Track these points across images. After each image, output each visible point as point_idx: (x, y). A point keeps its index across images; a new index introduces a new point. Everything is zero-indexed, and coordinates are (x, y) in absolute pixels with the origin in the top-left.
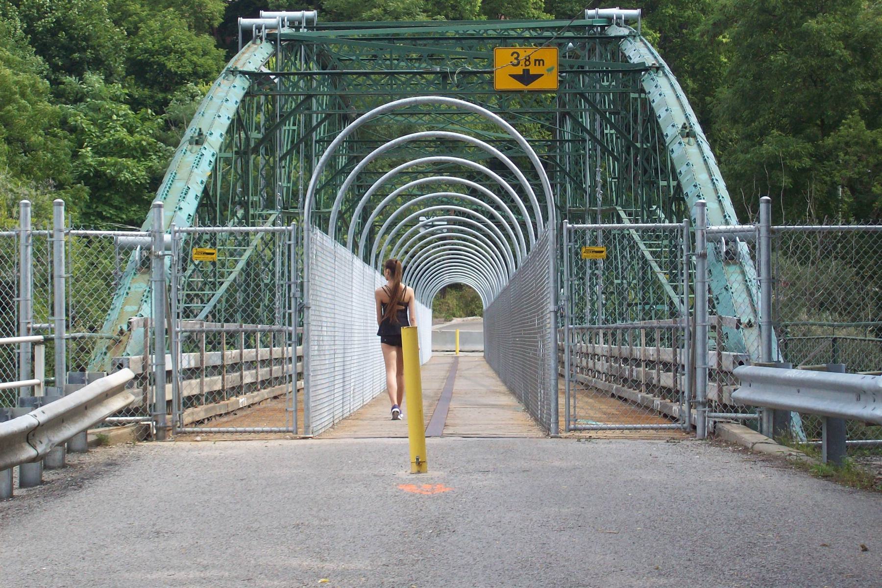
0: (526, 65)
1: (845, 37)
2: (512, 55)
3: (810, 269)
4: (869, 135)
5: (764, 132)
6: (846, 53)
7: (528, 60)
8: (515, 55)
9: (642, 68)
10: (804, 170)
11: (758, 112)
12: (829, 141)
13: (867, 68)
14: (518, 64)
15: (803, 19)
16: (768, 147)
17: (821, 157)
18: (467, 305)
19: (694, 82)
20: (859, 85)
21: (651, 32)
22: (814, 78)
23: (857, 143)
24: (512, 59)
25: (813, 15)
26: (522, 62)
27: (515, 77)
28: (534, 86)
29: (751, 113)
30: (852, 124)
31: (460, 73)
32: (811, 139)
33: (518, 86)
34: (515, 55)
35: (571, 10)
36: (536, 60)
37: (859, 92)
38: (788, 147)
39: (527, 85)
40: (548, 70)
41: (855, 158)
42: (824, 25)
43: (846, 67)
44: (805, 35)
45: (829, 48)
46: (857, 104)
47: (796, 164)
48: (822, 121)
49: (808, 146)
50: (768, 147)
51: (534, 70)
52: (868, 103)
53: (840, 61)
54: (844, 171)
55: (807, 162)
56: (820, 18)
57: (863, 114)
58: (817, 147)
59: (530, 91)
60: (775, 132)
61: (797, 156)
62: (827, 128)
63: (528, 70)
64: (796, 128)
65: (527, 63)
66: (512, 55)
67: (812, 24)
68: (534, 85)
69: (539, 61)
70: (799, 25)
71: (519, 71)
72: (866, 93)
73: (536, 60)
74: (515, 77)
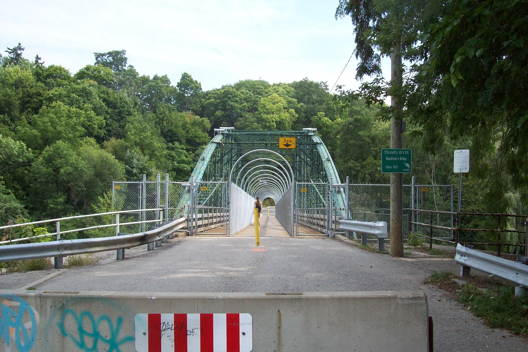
1: (369, 136)
10: (359, 170)
17: (363, 167)
18: (271, 203)
20: (372, 149)
22: (360, 147)
32: (360, 162)
44: (358, 136)
50: (350, 164)
55: (359, 168)
61: (357, 167)
62: (364, 159)
64: (356, 160)
67: (361, 133)
72: (374, 150)
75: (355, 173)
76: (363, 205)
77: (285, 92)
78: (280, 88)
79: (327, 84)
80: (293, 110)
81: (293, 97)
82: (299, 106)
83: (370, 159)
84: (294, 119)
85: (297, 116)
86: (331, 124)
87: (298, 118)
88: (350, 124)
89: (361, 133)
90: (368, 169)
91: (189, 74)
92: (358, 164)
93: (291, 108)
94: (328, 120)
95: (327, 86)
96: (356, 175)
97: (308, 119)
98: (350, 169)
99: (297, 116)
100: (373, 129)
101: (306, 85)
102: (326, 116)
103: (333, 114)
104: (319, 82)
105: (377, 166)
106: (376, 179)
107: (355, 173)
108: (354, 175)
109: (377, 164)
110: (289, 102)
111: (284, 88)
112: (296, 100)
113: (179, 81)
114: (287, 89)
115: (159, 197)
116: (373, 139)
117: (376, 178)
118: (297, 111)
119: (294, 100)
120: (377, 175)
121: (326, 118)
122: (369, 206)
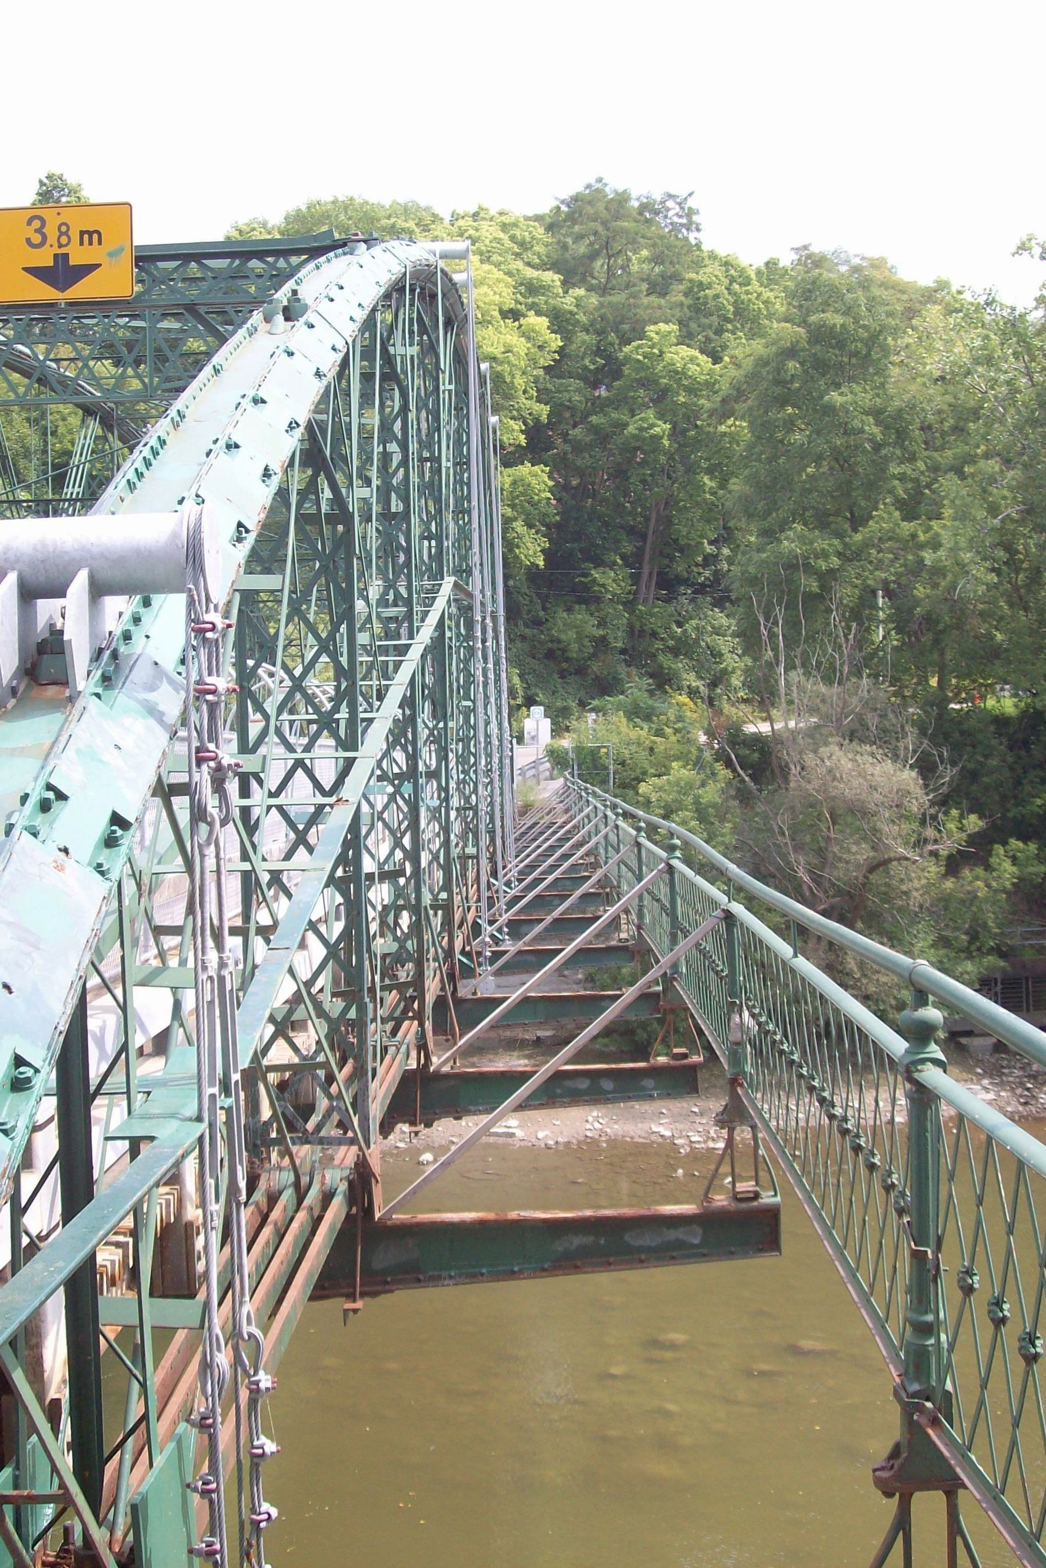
0: (60, 246)
1: (876, 413)
2: (30, 222)
3: (836, 689)
4: (907, 527)
5: (784, 525)
6: (876, 430)
7: (66, 233)
8: (37, 224)
10: (831, 572)
11: (776, 504)
12: (858, 537)
13: (904, 448)
14: (43, 243)
15: (826, 392)
16: (790, 544)
17: (851, 556)
19: (711, 480)
20: (895, 469)
21: (660, 423)
22: (841, 459)
23: (890, 539)
25: (837, 386)
26: (52, 239)
27: (36, 272)
28: (81, 290)
29: (1016, 687)
30: (885, 516)
32: (840, 535)
34: (37, 224)
35: (570, 401)
37: (894, 476)
38: (812, 543)
39: (63, 290)
40: (111, 255)
41: (891, 556)
42: (850, 397)
43: (877, 447)
44: (830, 410)
45: (856, 423)
46: (891, 492)
47: (823, 565)
48: (852, 514)
49: (836, 542)
50: (790, 544)
51: (78, 256)
52: (905, 491)
53: (870, 441)
54: (877, 573)
55: (835, 562)
56: (843, 389)
57: (900, 504)
58: (846, 545)
59: (73, 304)
60: (798, 527)
61: (824, 555)
62: (857, 522)
64: (822, 522)
65: (64, 240)
66: (30, 222)
67: (835, 397)
68: (83, 290)
69: (90, 234)
70: (821, 397)
71: (45, 258)
72: (902, 478)
74: (36, 272)
75: (815, 587)
76: (855, 734)
77: (508, 244)
78: (485, 225)
79: (691, 203)
80: (541, 323)
81: (543, 266)
82: (568, 302)
83: (886, 518)
84: (546, 360)
85: (556, 342)
86: (711, 373)
87: (561, 351)
88: (791, 352)
89: (835, 397)
90: (879, 565)
91: (71, 179)
92: (822, 543)
93: (539, 313)
94: (692, 359)
95: (691, 213)
96: (820, 597)
97: (609, 358)
98: (792, 565)
99: (556, 342)
100: (895, 371)
101: (601, 206)
102: (686, 338)
103: (719, 332)
104: (657, 196)
105: (922, 547)
106: (847, 540)
107: (815, 587)
108: (810, 598)
109: (922, 537)
110: (532, 288)
111: (504, 227)
112: (557, 277)
114: (517, 233)
115: (502, 620)
116: (896, 425)
117: (917, 602)
118: (560, 321)
119: (552, 278)
120: (920, 591)
121: (685, 351)
122: (885, 740)
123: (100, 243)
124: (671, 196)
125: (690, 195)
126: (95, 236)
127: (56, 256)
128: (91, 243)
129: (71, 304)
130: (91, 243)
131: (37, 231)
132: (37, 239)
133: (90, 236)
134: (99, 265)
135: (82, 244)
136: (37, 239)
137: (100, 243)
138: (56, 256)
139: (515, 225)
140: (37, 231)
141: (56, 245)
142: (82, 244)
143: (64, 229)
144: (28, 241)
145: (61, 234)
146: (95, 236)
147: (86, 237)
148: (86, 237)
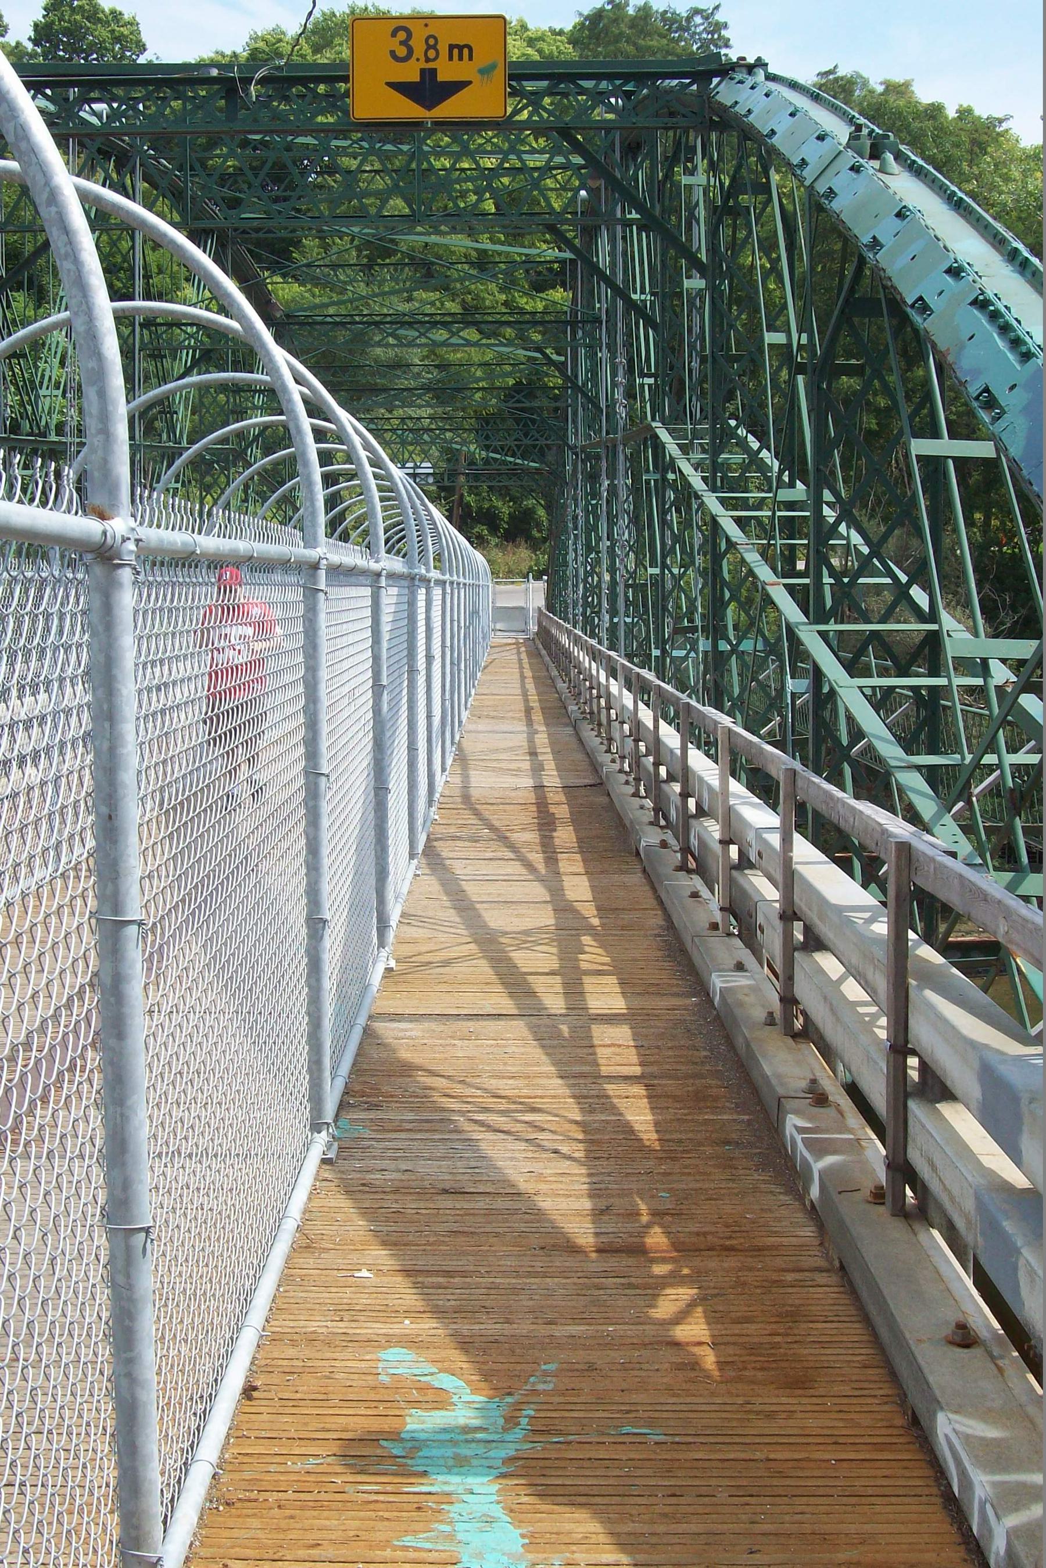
0: (428, 60)
2: (394, 34)
7: (434, 47)
8: (402, 35)
9: (713, 67)
24: (395, 44)
31: (262, 81)
33: (408, 109)
34: (402, 35)
36: (452, 47)
39: (429, 108)
51: (447, 71)
63: (433, 72)
65: (431, 54)
66: (394, 34)
69: (461, 48)
71: (411, 73)
73: (452, 47)
79: (719, 17)
113: (39, 15)
123: (471, 58)
124: (697, 11)
125: (717, 8)
126: (466, 51)
127: (423, 71)
128: (461, 58)
129: (436, 124)
130: (461, 58)
131: (401, 43)
132: (402, 52)
133: (460, 50)
134: (470, 83)
135: (451, 58)
136: (402, 52)
137: (471, 58)
138: (423, 71)
139: (541, 39)
140: (401, 43)
141: (423, 58)
142: (451, 58)
143: (432, 42)
144: (393, 54)
145: (429, 47)
146: (466, 51)
147: (456, 51)
148: (456, 51)
